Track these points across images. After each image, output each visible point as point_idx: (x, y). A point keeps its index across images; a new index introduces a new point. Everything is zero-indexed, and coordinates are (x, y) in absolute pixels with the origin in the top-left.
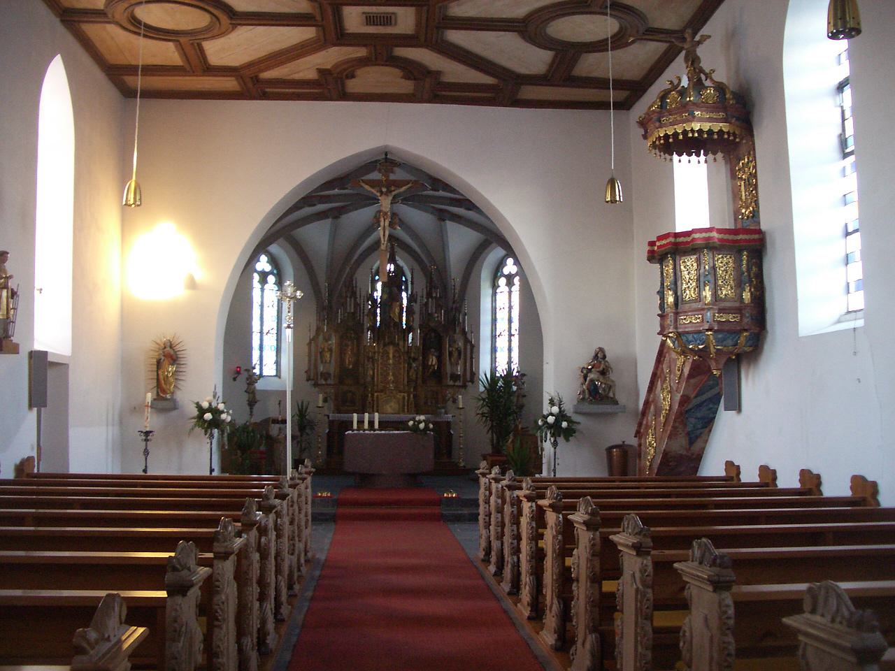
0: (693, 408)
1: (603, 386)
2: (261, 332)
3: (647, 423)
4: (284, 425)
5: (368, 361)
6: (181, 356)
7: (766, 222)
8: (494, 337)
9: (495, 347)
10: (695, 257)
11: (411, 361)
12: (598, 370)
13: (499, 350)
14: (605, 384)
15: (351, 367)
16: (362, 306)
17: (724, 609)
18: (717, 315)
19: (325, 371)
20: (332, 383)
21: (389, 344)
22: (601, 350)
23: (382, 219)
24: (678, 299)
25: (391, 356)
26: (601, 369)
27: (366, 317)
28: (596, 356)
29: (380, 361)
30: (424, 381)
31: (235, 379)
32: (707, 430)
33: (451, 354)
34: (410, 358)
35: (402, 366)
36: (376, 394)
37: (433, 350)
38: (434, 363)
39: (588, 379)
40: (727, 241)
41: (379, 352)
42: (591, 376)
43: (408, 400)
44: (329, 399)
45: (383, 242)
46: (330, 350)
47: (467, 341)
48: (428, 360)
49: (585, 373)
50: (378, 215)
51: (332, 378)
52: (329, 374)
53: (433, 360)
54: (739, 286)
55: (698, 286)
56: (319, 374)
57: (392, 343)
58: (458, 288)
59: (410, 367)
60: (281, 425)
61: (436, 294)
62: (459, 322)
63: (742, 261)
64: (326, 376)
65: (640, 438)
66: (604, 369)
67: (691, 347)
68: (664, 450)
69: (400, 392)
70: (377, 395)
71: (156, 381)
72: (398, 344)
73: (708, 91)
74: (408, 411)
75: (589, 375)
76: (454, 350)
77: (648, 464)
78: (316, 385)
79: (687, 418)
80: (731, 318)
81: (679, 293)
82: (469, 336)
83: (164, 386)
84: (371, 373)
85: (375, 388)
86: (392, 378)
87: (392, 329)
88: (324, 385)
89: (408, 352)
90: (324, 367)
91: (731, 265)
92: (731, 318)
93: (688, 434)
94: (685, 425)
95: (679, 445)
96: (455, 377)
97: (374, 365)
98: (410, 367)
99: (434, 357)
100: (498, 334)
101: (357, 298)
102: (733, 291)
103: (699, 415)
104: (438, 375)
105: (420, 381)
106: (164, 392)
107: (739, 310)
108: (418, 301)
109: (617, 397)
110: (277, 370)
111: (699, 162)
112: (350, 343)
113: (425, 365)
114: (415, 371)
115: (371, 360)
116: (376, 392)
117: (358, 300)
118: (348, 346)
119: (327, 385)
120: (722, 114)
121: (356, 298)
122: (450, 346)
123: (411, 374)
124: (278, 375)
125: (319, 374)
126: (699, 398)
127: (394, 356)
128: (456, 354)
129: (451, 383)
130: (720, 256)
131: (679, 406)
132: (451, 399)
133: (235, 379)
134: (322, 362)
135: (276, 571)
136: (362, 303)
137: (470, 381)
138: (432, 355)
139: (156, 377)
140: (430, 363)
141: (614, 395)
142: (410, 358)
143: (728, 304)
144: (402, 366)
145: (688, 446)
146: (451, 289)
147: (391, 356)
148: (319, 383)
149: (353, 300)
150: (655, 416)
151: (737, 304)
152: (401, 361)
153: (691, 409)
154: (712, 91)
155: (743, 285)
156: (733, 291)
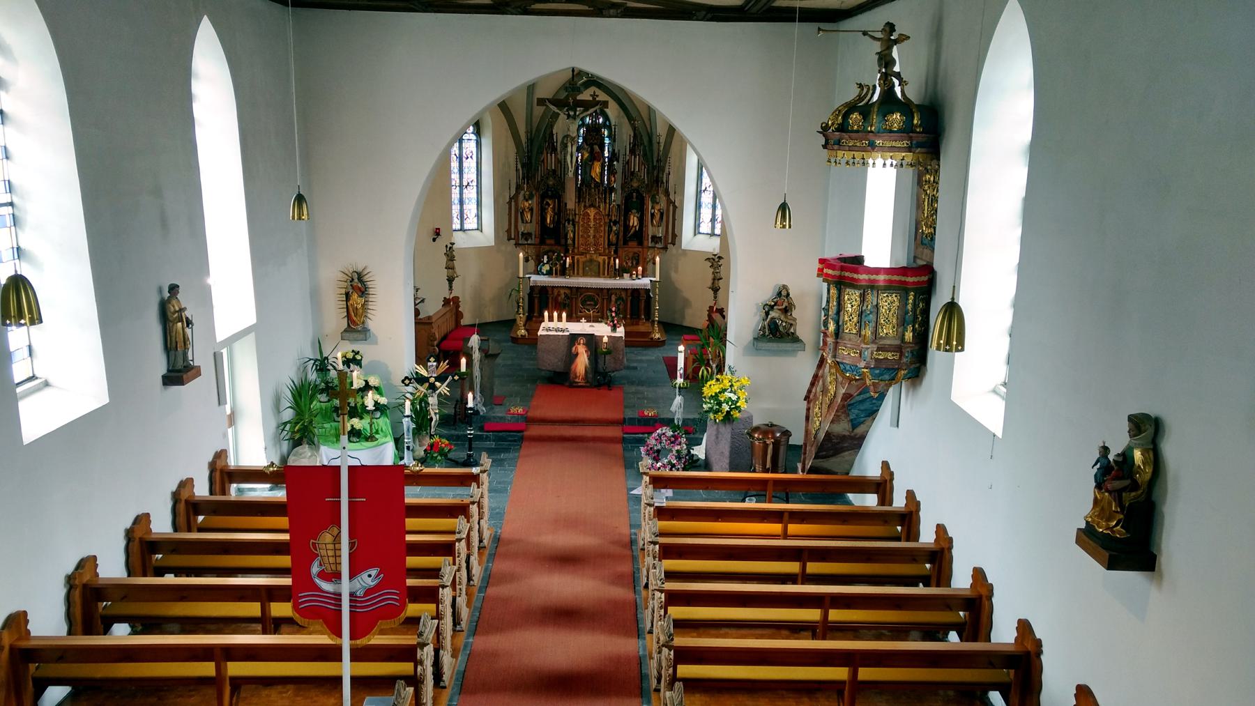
0: (856, 403)
1: (784, 324)
2: (461, 186)
3: (815, 393)
5: (569, 224)
6: (370, 286)
7: (941, 264)
8: (699, 193)
9: (700, 203)
10: (860, 292)
11: (612, 224)
12: (780, 307)
13: (703, 205)
14: (786, 322)
18: (875, 353)
19: (526, 232)
20: (533, 242)
21: (590, 206)
22: (785, 287)
23: (569, 145)
24: (839, 329)
25: (592, 217)
26: (784, 307)
28: (779, 294)
30: (625, 243)
31: (434, 240)
32: (871, 418)
33: (653, 215)
34: (611, 220)
35: (602, 229)
36: (576, 257)
38: (636, 224)
39: (769, 316)
40: (895, 281)
41: (580, 215)
42: (773, 314)
43: (609, 263)
44: (530, 258)
45: (570, 169)
46: (531, 210)
47: (670, 202)
49: (768, 308)
50: (565, 142)
51: (533, 237)
53: (634, 221)
54: (902, 323)
55: (860, 322)
56: (520, 233)
57: (592, 206)
58: (662, 140)
59: (610, 231)
61: (640, 151)
62: (662, 182)
63: (908, 299)
64: (527, 236)
65: (809, 403)
66: (786, 307)
67: (848, 375)
68: (827, 431)
69: (600, 255)
70: (578, 258)
71: (345, 310)
72: (599, 207)
73: (894, 117)
74: (608, 274)
75: (770, 312)
77: (814, 432)
78: (517, 245)
79: (850, 410)
80: (889, 356)
81: (840, 323)
82: (672, 197)
83: (355, 318)
85: (576, 251)
86: (593, 241)
87: (593, 190)
89: (609, 215)
90: (525, 227)
91: (897, 303)
92: (889, 356)
93: (851, 420)
94: (848, 415)
95: (843, 428)
96: (655, 239)
97: (574, 227)
98: (610, 231)
99: (635, 218)
100: (703, 188)
102: (895, 330)
103: (862, 408)
104: (639, 236)
106: (354, 322)
107: (899, 349)
108: (621, 159)
109: (798, 333)
110: (478, 223)
111: (884, 164)
113: (627, 227)
114: (615, 234)
116: (577, 255)
118: (549, 205)
119: (528, 244)
120: (905, 143)
122: (653, 208)
123: (611, 237)
124: (480, 229)
125: (520, 233)
126: (862, 396)
128: (658, 217)
129: (653, 245)
130: (885, 295)
131: (841, 401)
132: (652, 261)
133: (434, 240)
134: (523, 222)
137: (671, 243)
139: (345, 306)
140: (631, 224)
141: (795, 330)
142: (611, 220)
143: (888, 342)
145: (851, 430)
147: (592, 217)
148: (520, 242)
150: (822, 391)
151: (898, 342)
153: (854, 403)
154: (898, 117)
155: (905, 325)
156: (895, 330)
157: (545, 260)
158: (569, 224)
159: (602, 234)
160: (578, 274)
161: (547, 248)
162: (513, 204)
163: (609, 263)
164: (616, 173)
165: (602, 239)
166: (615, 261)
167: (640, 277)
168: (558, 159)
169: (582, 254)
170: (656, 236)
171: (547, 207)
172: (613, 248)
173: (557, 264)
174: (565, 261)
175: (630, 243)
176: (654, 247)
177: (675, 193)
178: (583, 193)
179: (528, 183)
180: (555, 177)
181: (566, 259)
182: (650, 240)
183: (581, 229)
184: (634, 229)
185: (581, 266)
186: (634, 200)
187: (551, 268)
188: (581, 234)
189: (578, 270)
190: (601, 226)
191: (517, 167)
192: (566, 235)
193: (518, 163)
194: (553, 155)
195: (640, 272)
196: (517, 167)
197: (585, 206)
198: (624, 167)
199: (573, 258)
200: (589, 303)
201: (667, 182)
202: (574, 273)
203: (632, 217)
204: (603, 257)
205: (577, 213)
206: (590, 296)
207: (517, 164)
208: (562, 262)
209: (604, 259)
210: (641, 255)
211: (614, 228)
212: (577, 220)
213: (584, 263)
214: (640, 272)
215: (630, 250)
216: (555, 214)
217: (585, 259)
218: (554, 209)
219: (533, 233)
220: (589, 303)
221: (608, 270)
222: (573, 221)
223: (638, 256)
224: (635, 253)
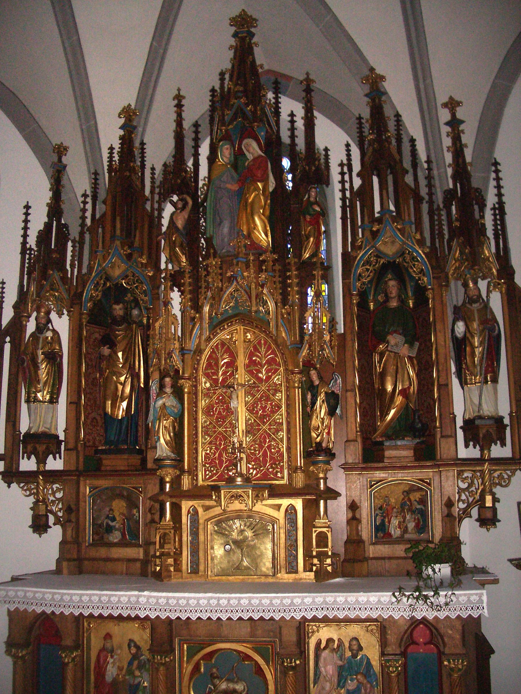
36: (186, 505)
204: (285, 502)
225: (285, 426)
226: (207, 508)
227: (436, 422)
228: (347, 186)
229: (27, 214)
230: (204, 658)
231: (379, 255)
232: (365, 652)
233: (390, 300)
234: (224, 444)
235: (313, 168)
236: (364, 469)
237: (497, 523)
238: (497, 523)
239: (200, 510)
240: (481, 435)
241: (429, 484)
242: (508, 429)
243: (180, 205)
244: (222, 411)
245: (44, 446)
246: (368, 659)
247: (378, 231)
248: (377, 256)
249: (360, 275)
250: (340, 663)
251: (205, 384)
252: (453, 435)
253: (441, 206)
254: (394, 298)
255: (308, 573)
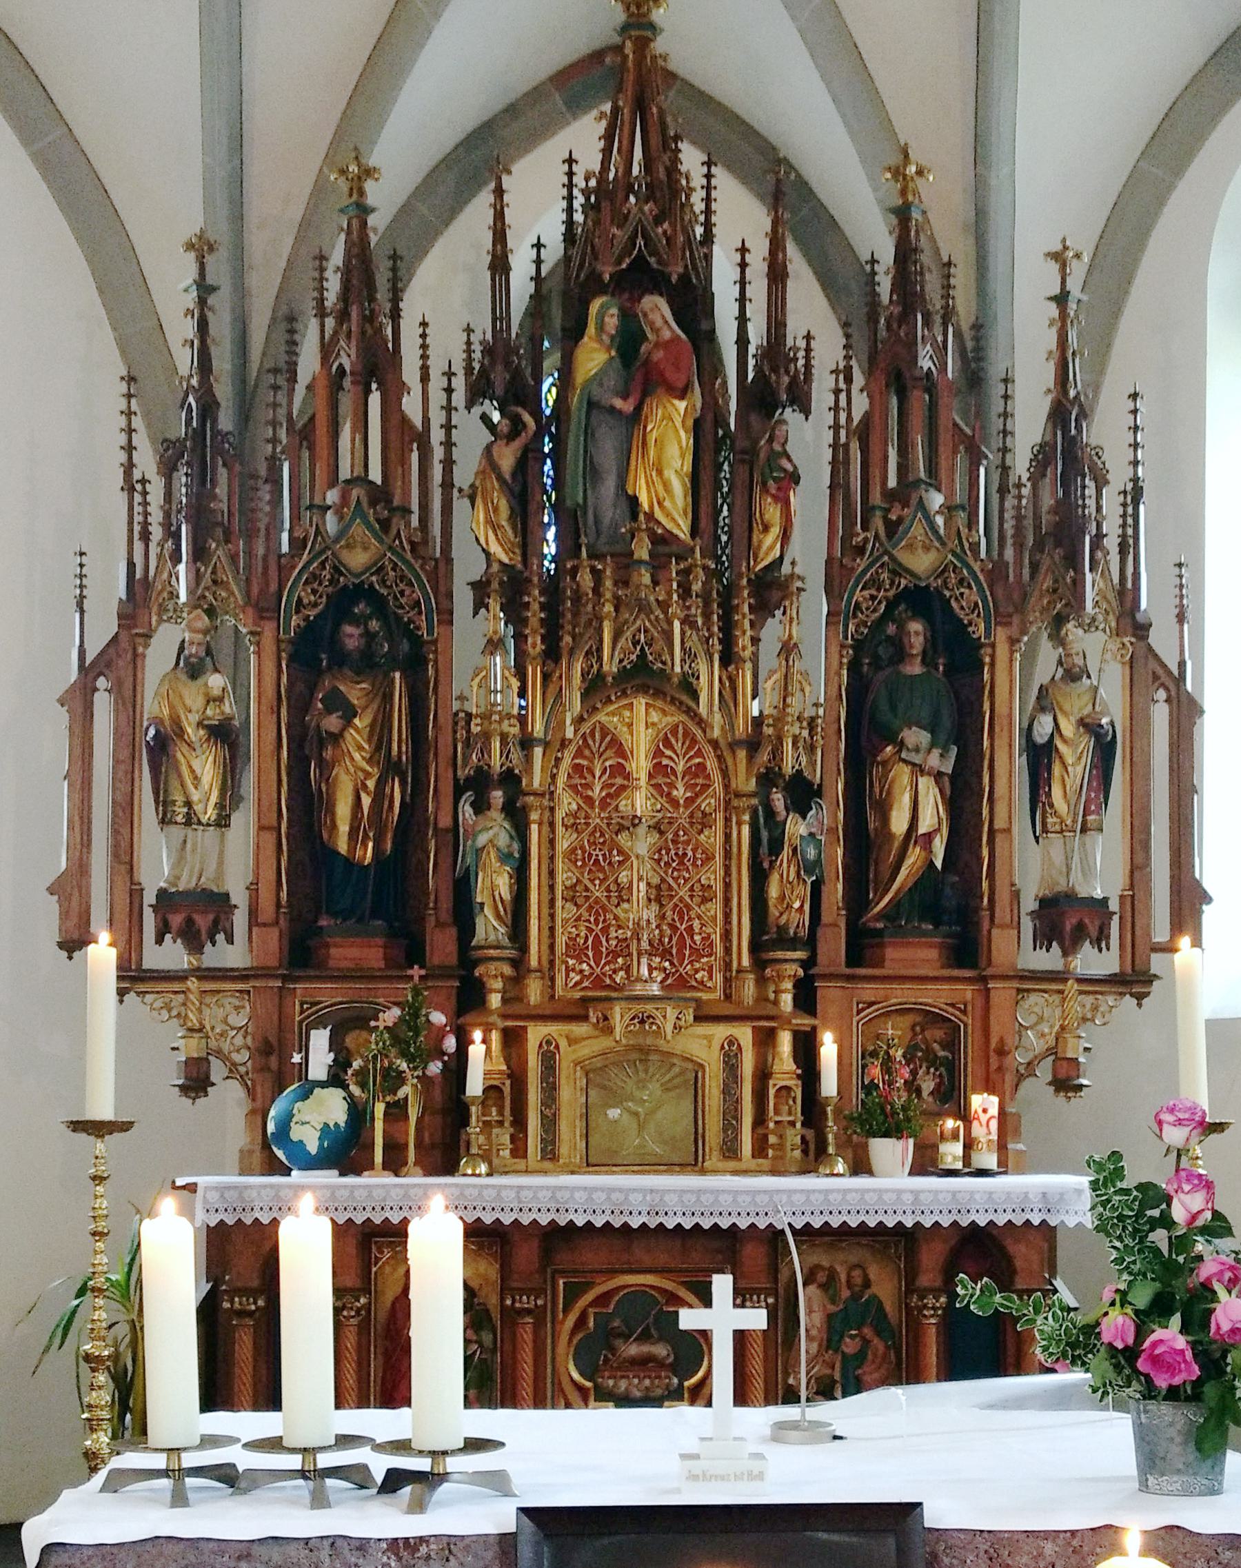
4: (257, 1167)
5: (480, 807)
11: (778, 800)
15: (367, 854)
16: (437, 435)
17: (781, 495)
19: (186, 883)
25: (640, 765)
27: (461, 506)
29: (567, 803)
35: (713, 838)
36: (536, 1034)
37: (916, 736)
43: (763, 1075)
44: (217, 1070)
48: (884, 809)
51: (240, 920)
52: (219, 903)
60: (700, 1013)
74: (760, 1149)
76: (1068, 728)
82: (1161, 640)
84: (504, 884)
86: (650, 914)
88: (180, 977)
99: (927, 785)
101: (402, 388)
105: (833, 946)
112: (355, 693)
115: (497, 796)
117: (411, 406)
118: (349, 713)
121: (393, 393)
123: (773, 891)
127: (659, 770)
132: (1045, 1071)
134: (165, 821)
135: (777, 1310)
136: (437, 418)
138: (918, 769)
140: (899, 823)
142: (768, 779)
144: (713, 838)
146: (1078, 506)
147: (640, 765)
149: (375, 399)
152: (707, 803)
157: (320, 1059)
158: (480, 807)
159: (712, 876)
160: (550, 1153)
161: (330, 994)
162: (103, 704)
163: (763, 1075)
164: (795, 478)
165: (716, 908)
166: (806, 1049)
167: (990, 1160)
168: (405, 421)
169: (575, 1013)
170: (1070, 897)
171: (332, 723)
172: (790, 965)
173: (400, 1079)
174: (458, 1067)
175: (897, 956)
176: (1058, 977)
177: (1181, 618)
178: (577, 598)
179: (199, 554)
180: (385, 525)
181: (464, 1043)
182: (1027, 926)
183: (563, 844)
184: (914, 856)
185: (569, 1094)
186: (915, 668)
187: (358, 1115)
188: (564, 876)
189: (550, 1123)
190: (705, 822)
191: (129, 467)
192: (463, 887)
193: (141, 439)
194: (375, 399)
195: (985, 1130)
196: (129, 467)
197: (594, 687)
198: (839, 451)
199: (513, 1040)
200: (633, 1350)
201: (1127, 546)
202: (519, 1150)
203: (902, 774)
204: (721, 1032)
205: (538, 729)
206: (640, 1294)
207: (130, 448)
208: (435, 1068)
209: (732, 1041)
210: (970, 1022)
211: (796, 828)
212: (537, 780)
213: (592, 1073)
214: (985, 1130)
215: (901, 994)
216: (390, 768)
217: (605, 1043)
218: (380, 734)
219: (239, 897)
220: (633, 1350)
221: (760, 1120)
222: (510, 779)
223: (951, 1043)
224: (932, 1018)
225: (720, 895)
226: (572, 1041)
227: (982, 898)
228: (843, 421)
229: (424, 336)
230: (594, 1303)
231: (898, 570)
232: (874, 1289)
233: (907, 660)
234: (604, 921)
235: (553, 429)
236: (849, 978)
237: (209, 1089)
238: (209, 1089)
239: (563, 1043)
240: (1068, 928)
241: (964, 1012)
242: (1116, 918)
243: (505, 427)
244: (601, 858)
245: (211, 917)
246: (880, 1303)
247: (900, 520)
248: (894, 573)
249: (858, 606)
250: (832, 1308)
251: (567, 803)
252: (1015, 923)
253: (1024, 480)
254: (917, 655)
255: (760, 1161)
